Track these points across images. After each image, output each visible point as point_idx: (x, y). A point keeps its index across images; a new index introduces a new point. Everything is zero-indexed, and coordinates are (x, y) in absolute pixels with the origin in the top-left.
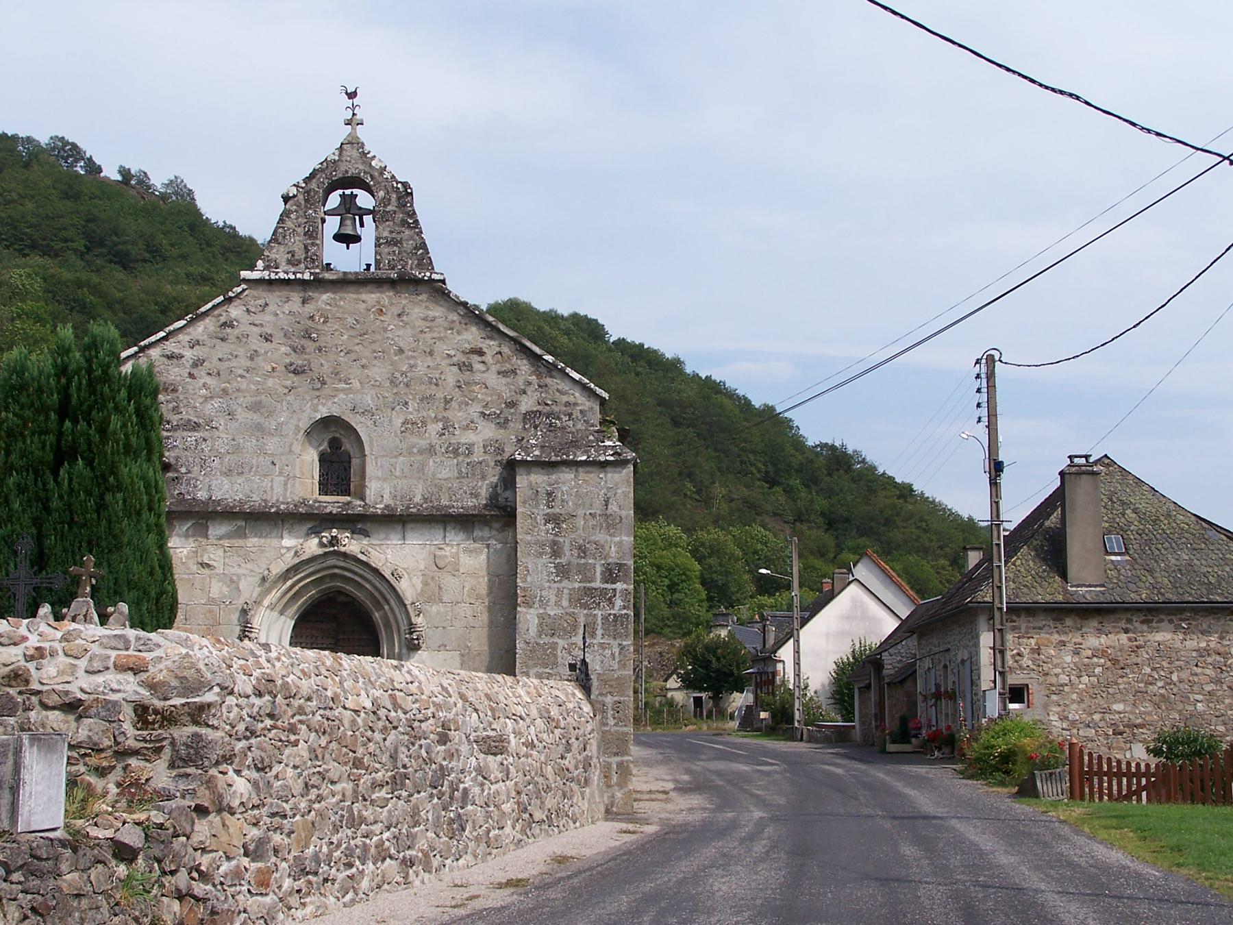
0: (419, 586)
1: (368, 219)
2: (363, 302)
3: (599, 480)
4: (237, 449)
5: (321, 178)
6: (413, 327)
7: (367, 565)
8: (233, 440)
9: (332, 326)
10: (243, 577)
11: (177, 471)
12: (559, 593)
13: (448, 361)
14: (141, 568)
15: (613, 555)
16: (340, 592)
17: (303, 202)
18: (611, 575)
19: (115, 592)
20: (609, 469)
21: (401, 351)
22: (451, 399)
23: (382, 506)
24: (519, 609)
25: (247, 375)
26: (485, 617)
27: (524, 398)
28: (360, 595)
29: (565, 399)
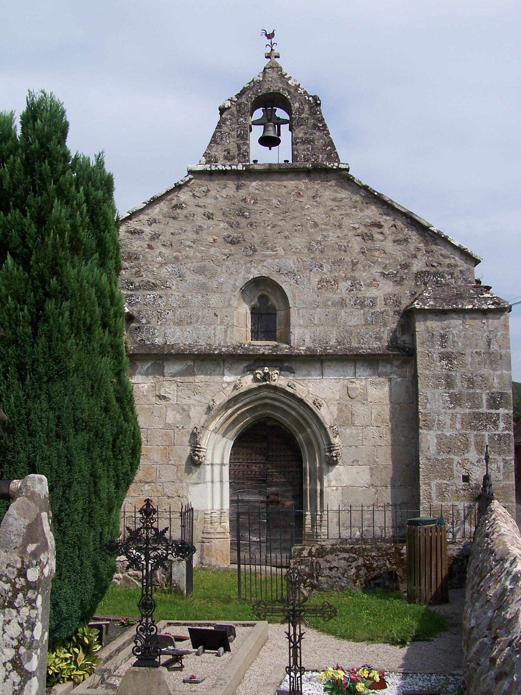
0: (335, 413)
1: (285, 128)
2: (285, 187)
3: (482, 325)
4: (187, 304)
5: (250, 94)
6: (325, 206)
7: (293, 396)
8: (184, 296)
9: (261, 206)
10: (192, 407)
11: (139, 322)
12: (453, 417)
13: (353, 232)
14: (92, 401)
15: (496, 385)
16: (269, 418)
17: (236, 113)
18: (494, 401)
19: (58, 436)
20: (490, 316)
21: (316, 225)
22: (357, 262)
23: (304, 348)
24: (420, 431)
25: (194, 246)
26: (389, 437)
27: (415, 262)
28: (287, 421)
29: (447, 261)
